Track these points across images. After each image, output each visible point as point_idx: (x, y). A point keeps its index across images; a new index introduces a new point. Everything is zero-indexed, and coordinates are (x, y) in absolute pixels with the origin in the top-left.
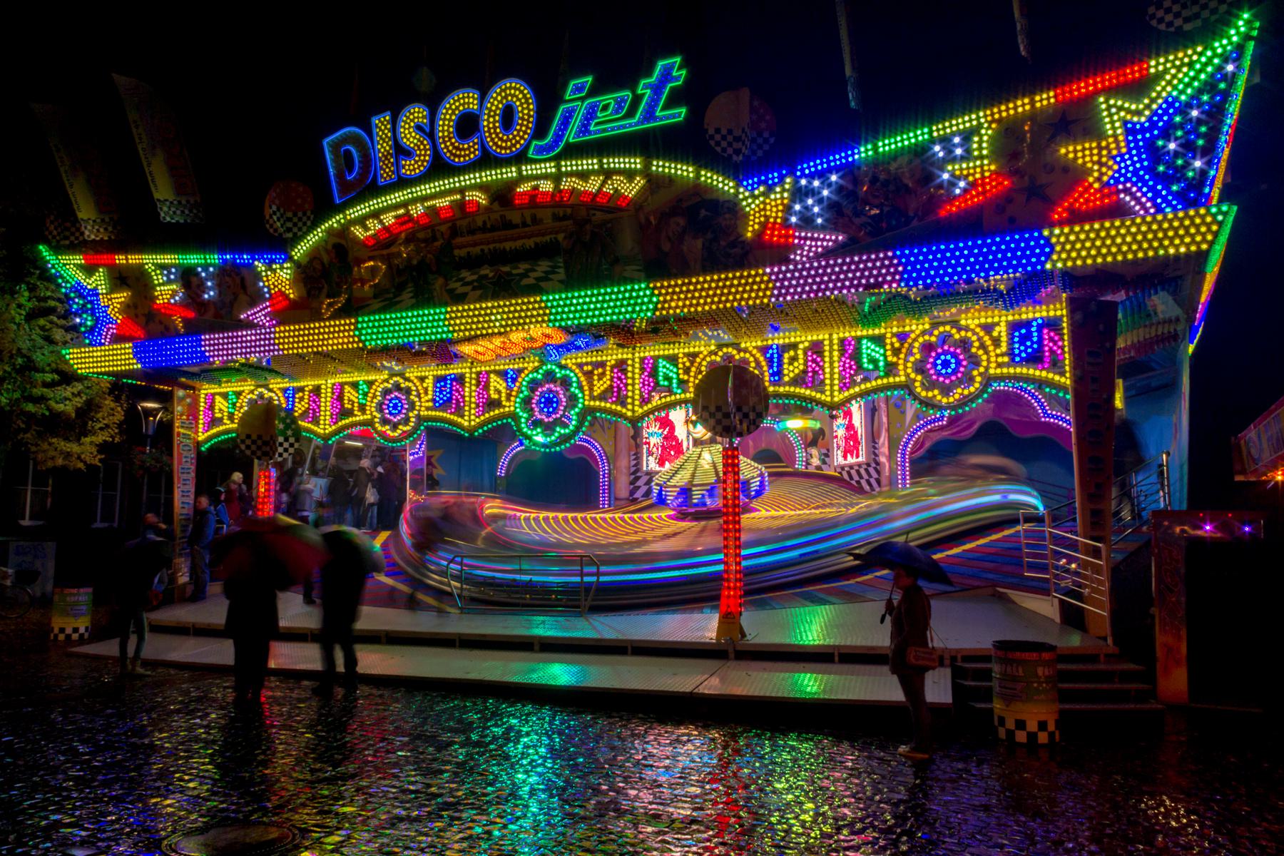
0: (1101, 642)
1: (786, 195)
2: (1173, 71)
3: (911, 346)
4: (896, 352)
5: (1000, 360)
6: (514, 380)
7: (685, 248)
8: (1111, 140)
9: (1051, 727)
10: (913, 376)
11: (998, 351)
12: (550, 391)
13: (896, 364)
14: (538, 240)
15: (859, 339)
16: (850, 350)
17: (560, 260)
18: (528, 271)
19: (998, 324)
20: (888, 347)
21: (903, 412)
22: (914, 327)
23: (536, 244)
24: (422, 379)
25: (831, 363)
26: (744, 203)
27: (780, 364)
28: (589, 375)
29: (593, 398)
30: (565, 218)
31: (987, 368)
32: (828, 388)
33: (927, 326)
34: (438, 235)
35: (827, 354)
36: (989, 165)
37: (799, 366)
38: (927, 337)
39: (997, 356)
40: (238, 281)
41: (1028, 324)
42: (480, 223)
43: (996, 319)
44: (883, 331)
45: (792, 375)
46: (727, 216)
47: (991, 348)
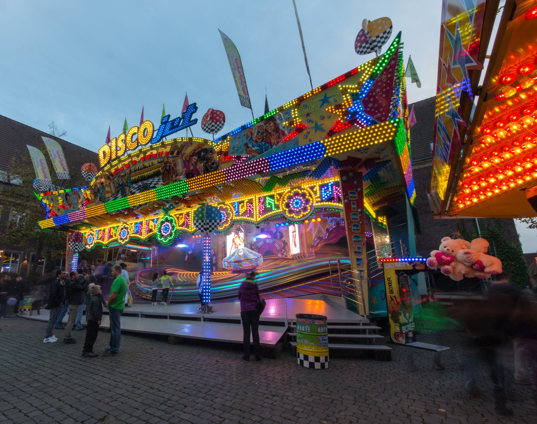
0: (363, 318)
1: (228, 143)
2: (368, 69)
3: (284, 198)
4: (278, 200)
5: (317, 200)
6: (156, 222)
7: (198, 167)
8: (346, 102)
9: (322, 360)
10: (285, 209)
11: (316, 197)
12: (167, 225)
13: (279, 205)
14: (154, 171)
15: (265, 197)
16: (262, 201)
17: (160, 176)
18: (152, 182)
19: (315, 186)
20: (276, 199)
21: (312, 235)
22: (285, 190)
23: (154, 172)
24: (131, 224)
25: (256, 207)
26: (215, 148)
27: (238, 208)
28: (178, 218)
29: (179, 226)
30: (161, 162)
31: (312, 204)
32: (255, 216)
33: (289, 190)
34: (127, 174)
35: (254, 203)
36: (299, 120)
37: (245, 209)
38: (289, 194)
39: (316, 198)
40: (78, 195)
41: (327, 185)
42: (137, 168)
43: (315, 184)
44: (273, 193)
45: (242, 212)
46: (210, 154)
47: (313, 196)
